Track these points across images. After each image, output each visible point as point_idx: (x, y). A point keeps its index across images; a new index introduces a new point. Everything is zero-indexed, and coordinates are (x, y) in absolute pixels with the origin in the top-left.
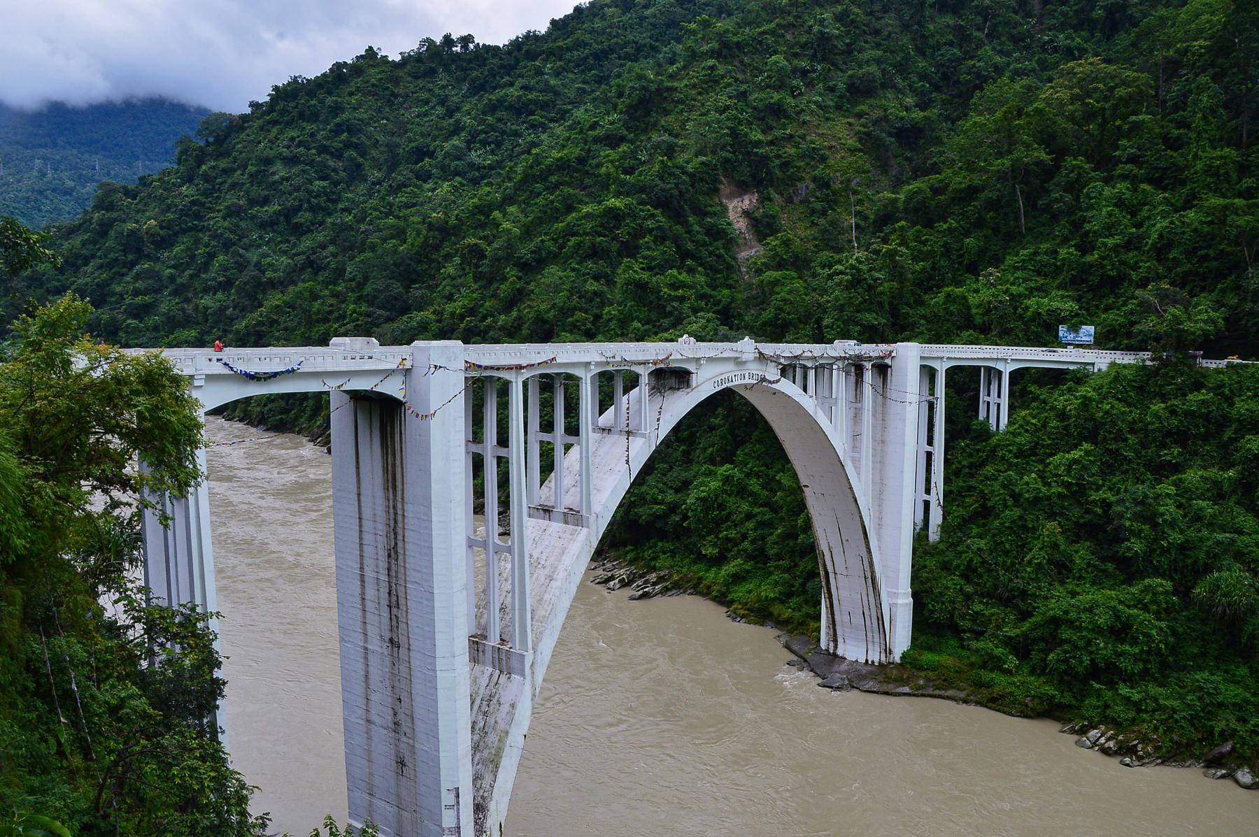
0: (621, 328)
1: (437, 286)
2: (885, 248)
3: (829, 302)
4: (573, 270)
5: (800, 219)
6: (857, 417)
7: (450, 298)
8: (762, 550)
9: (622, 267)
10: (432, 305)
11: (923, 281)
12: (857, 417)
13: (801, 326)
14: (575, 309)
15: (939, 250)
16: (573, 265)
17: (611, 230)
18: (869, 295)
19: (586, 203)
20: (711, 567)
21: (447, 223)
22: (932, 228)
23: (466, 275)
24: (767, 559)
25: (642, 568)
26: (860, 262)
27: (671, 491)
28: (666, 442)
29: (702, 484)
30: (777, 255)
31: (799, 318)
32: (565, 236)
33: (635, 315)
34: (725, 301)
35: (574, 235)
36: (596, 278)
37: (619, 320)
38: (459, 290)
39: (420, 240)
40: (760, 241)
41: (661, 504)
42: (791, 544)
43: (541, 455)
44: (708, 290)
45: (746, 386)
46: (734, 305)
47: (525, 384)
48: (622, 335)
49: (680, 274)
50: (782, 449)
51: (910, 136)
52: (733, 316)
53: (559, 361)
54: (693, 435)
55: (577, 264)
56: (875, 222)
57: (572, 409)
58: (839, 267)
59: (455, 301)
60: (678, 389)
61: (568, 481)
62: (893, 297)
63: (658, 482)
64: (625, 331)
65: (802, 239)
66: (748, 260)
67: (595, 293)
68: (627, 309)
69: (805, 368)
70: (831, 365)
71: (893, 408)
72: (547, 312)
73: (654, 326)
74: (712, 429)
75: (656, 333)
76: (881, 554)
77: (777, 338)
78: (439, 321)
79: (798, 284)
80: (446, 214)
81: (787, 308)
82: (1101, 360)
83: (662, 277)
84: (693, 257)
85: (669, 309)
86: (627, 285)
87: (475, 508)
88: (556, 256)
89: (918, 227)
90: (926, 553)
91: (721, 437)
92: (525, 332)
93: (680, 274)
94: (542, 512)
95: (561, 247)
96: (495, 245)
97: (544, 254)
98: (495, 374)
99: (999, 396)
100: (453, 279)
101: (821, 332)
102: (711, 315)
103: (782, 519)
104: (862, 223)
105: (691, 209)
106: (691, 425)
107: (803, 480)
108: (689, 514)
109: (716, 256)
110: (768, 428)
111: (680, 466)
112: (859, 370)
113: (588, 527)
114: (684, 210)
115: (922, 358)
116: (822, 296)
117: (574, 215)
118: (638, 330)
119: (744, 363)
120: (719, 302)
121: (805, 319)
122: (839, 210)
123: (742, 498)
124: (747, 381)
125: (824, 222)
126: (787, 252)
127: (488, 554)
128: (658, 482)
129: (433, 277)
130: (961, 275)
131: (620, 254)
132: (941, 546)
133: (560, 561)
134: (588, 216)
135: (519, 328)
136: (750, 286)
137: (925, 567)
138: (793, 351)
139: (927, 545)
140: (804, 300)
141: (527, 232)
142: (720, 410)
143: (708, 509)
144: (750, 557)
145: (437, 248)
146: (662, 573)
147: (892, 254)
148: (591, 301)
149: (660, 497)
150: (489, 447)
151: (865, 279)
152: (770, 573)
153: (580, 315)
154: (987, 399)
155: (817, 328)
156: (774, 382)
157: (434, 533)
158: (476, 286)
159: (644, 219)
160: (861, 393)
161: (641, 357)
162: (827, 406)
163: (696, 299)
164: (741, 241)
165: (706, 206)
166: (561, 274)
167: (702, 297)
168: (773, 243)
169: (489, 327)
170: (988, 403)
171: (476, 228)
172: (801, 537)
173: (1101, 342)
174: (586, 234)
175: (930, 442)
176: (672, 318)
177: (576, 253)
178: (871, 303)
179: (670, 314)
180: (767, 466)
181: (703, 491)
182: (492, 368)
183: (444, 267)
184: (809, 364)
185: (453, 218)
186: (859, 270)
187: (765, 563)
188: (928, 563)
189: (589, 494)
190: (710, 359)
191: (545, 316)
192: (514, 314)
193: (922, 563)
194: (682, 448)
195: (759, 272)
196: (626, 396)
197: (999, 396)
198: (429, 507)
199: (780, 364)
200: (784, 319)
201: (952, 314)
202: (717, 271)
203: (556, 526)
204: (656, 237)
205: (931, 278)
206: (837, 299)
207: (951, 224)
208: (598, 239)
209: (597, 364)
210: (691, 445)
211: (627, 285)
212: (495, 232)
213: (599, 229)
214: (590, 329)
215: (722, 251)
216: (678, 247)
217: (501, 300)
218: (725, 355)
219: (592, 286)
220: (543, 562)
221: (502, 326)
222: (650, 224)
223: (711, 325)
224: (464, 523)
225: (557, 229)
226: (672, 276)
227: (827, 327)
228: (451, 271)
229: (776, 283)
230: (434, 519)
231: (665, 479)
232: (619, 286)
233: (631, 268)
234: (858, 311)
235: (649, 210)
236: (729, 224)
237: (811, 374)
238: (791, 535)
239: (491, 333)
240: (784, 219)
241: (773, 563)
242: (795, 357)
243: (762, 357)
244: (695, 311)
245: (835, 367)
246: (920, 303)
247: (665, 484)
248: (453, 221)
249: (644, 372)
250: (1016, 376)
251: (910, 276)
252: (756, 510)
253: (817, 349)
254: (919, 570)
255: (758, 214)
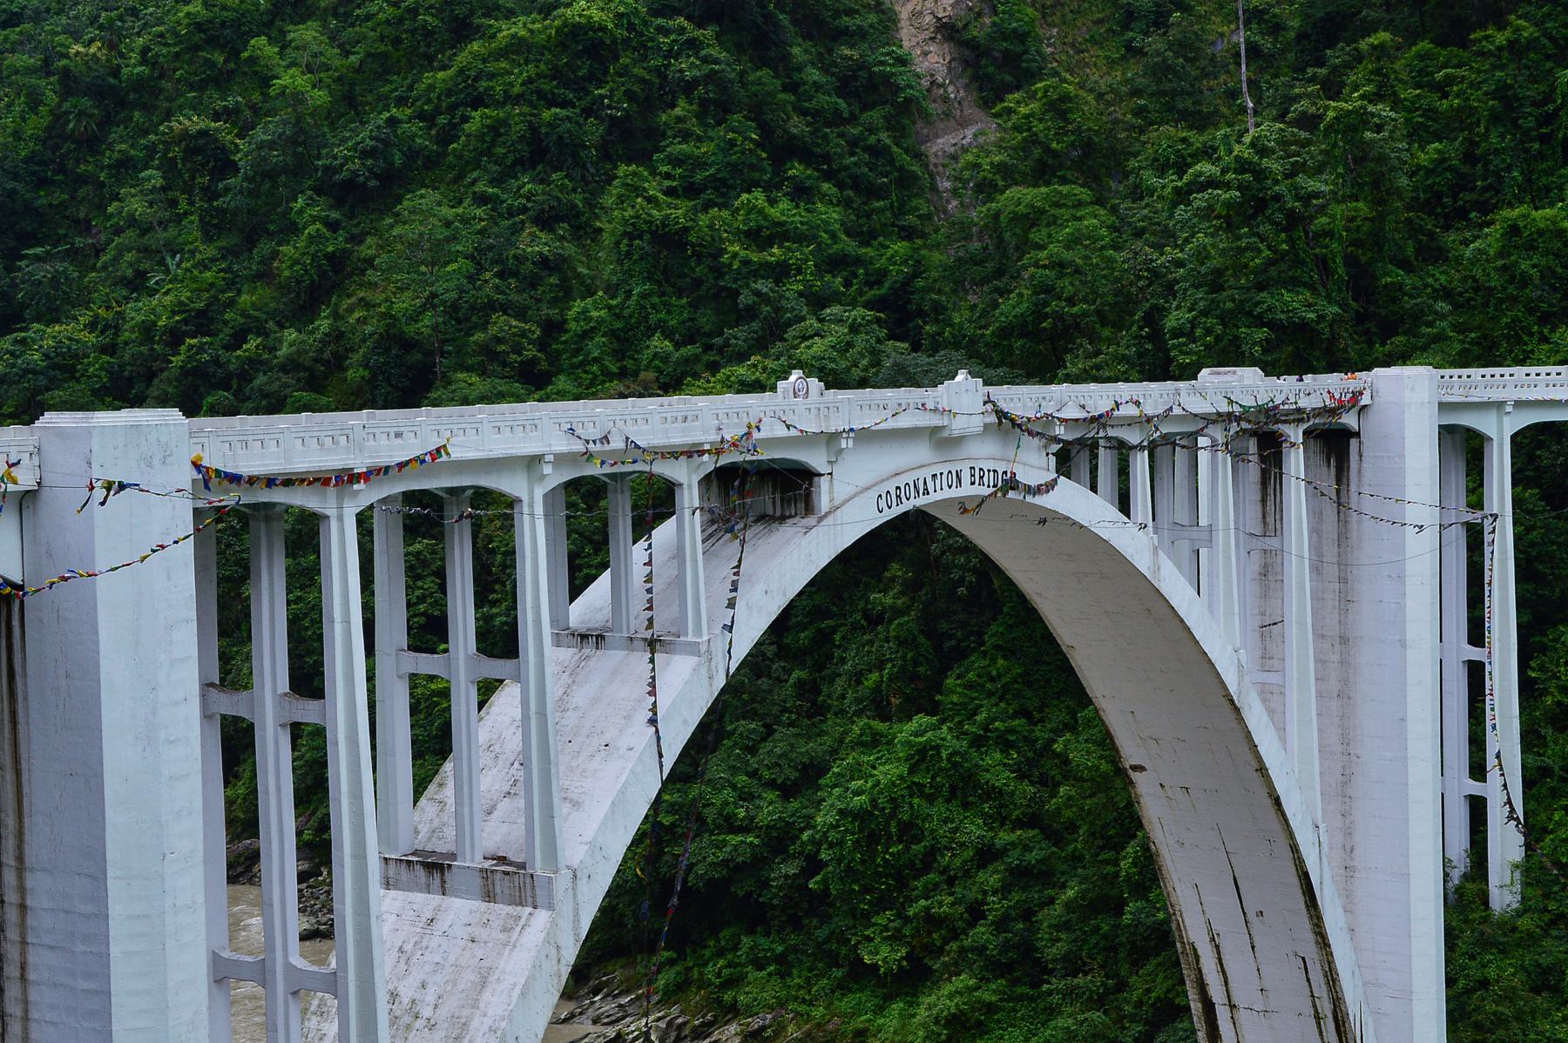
0: (619, 355)
1: (98, 252)
2: (1333, 109)
3: (1180, 264)
4: (482, 199)
5: (1093, 40)
6: (1268, 574)
7: (137, 284)
8: (1027, 948)
9: (616, 189)
10: (87, 304)
11: (1438, 196)
12: (1268, 574)
13: (1106, 333)
14: (491, 307)
15: (1482, 104)
16: (480, 187)
17: (581, 87)
18: (1291, 241)
19: (509, 14)
20: (889, 998)
21: (116, 72)
22: (1464, 43)
23: (178, 219)
24: (1039, 971)
25: (700, 1010)
26: (1263, 152)
27: (771, 795)
28: (756, 662)
29: (856, 771)
30: (1033, 140)
31: (1098, 312)
32: (453, 108)
33: (653, 318)
34: (897, 272)
35: (477, 103)
36: (546, 221)
37: (613, 334)
38: (162, 262)
39: (37, 123)
40: (986, 104)
41: (745, 830)
42: (1105, 928)
43: (414, 710)
44: (848, 245)
45: (963, 506)
46: (920, 283)
47: (364, 520)
48: (623, 374)
49: (772, 202)
50: (1066, 669)
52: (921, 313)
53: (457, 453)
54: (824, 638)
55: (492, 182)
56: (1302, 36)
58: (1206, 168)
59: (152, 293)
60: (783, 519)
61: (491, 781)
62: (1356, 243)
63: (734, 770)
64: (629, 363)
65: (1100, 96)
66: (954, 158)
67: (544, 262)
68: (632, 302)
69: (1123, 450)
70: (1193, 436)
71: (1369, 536)
72: (415, 318)
73: (708, 348)
74: (875, 620)
75: (714, 368)
76: (1356, 949)
77: (1043, 370)
78: (110, 349)
79: (1094, 221)
80: (112, 46)
81: (1067, 286)
83: (725, 213)
84: (807, 157)
85: (745, 299)
86: (632, 237)
87: (230, 866)
88: (432, 162)
89: (1424, 45)
90: (1485, 943)
91: (902, 642)
92: (354, 374)
93: (772, 202)
94: (420, 872)
95: (446, 137)
96: (260, 134)
97: (398, 160)
98: (279, 496)
100: (145, 231)
101: (1162, 348)
102: (859, 313)
103: (1076, 858)
104: (1266, 44)
105: (795, 22)
106: (819, 613)
107: (1130, 752)
108: (824, 856)
109: (869, 149)
110: (1027, 614)
111: (792, 724)
112: (1271, 448)
113: (550, 907)
114: (777, 25)
115: (1444, 407)
116: (1159, 248)
117: (475, 46)
118: (665, 359)
119: (958, 441)
120: (882, 274)
121: (1117, 314)
122: (1201, 9)
123: (966, 805)
124: (967, 490)
125: (1161, 46)
126: (1061, 133)
127: (271, 997)
128: (734, 770)
129: (84, 227)
130: (1550, 172)
131: (607, 154)
132: (1525, 923)
133: (475, 1006)
134: (518, 49)
135: (337, 363)
136: (963, 231)
137: (1484, 983)
138: (1089, 403)
139: (1486, 920)
140: (1111, 260)
141: (349, 102)
142: (895, 569)
143: (873, 838)
144: (995, 968)
145: (92, 143)
146: (756, 1023)
147: (1354, 124)
148: (533, 286)
149: (742, 813)
150: (462, 662)
151: (1278, 198)
152: (1052, 1012)
153: (502, 324)
155: (1149, 337)
156: (1037, 490)
157: (115, 951)
158: (209, 251)
159: (670, 54)
160: (1279, 509)
161: (678, 437)
162: (1185, 547)
163: (820, 270)
164: (934, 108)
165: (837, 14)
166: (447, 212)
167: (835, 263)
168: (1023, 110)
169: (255, 363)
171: (202, 87)
172: (1131, 906)
174: (517, 100)
176: (755, 325)
177: (488, 152)
178: (1298, 262)
179: (750, 313)
180: (1024, 713)
181: (858, 793)
182: (270, 482)
183: (116, 197)
184: (1133, 437)
185: (134, 57)
186: (1260, 174)
187: (1036, 985)
188: (1492, 973)
189: (549, 815)
190: (866, 436)
191: (410, 330)
192: (324, 324)
193: (1475, 972)
194: (797, 674)
195: (987, 189)
196: (642, 544)
198: (98, 877)
199: (1056, 440)
200: (1059, 317)
201: (1525, 282)
202: (874, 192)
203: (461, 910)
204: (704, 103)
205: (1462, 184)
206: (1201, 255)
207: (1518, 29)
208: (547, 115)
209: (561, 459)
210: (821, 667)
211: (632, 237)
212: (256, 97)
213: (546, 86)
214: (534, 361)
215: (885, 137)
216: (766, 129)
217: (284, 288)
218: (905, 421)
219: (535, 243)
220: (427, 1012)
221: (289, 358)
222: (687, 67)
223: (860, 341)
224: (201, 916)
225: (431, 87)
226: (751, 209)
227: (1177, 333)
228: (136, 205)
229: (1032, 218)
230: (116, 909)
231: (753, 762)
232: (607, 239)
233: (638, 190)
234: (1260, 287)
235: (682, 30)
236: (902, 61)
237: (1140, 463)
238: (1106, 903)
239: (260, 380)
240: (1050, 42)
241: (1056, 983)
242: (1093, 419)
243: (1006, 424)
244: (818, 302)
245: (1203, 441)
246: (1435, 254)
247: (753, 774)
248: (133, 68)
249: (687, 477)
251: (1404, 181)
252: (1005, 837)
253: (1154, 396)
254: (1469, 991)
255: (979, 31)
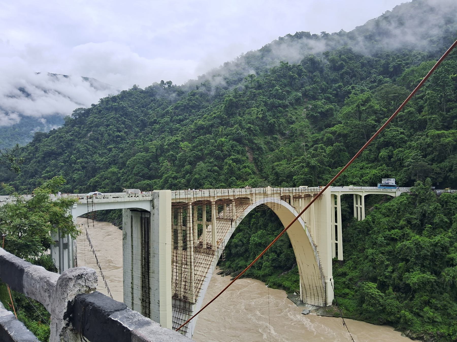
51: (326, 114)
57: (209, 213)
82: (397, 192)
99: (361, 205)
154: (357, 206)
170: (357, 207)
173: (399, 184)
175: (336, 222)
197: (361, 205)
250: (366, 197)
